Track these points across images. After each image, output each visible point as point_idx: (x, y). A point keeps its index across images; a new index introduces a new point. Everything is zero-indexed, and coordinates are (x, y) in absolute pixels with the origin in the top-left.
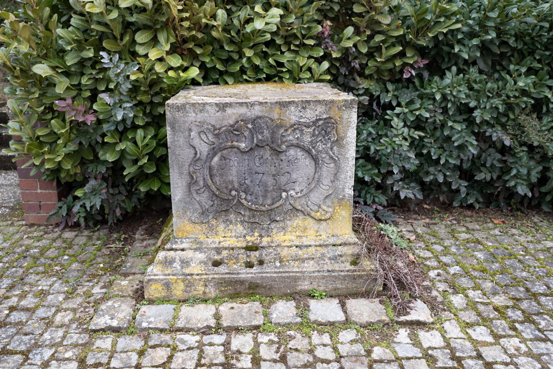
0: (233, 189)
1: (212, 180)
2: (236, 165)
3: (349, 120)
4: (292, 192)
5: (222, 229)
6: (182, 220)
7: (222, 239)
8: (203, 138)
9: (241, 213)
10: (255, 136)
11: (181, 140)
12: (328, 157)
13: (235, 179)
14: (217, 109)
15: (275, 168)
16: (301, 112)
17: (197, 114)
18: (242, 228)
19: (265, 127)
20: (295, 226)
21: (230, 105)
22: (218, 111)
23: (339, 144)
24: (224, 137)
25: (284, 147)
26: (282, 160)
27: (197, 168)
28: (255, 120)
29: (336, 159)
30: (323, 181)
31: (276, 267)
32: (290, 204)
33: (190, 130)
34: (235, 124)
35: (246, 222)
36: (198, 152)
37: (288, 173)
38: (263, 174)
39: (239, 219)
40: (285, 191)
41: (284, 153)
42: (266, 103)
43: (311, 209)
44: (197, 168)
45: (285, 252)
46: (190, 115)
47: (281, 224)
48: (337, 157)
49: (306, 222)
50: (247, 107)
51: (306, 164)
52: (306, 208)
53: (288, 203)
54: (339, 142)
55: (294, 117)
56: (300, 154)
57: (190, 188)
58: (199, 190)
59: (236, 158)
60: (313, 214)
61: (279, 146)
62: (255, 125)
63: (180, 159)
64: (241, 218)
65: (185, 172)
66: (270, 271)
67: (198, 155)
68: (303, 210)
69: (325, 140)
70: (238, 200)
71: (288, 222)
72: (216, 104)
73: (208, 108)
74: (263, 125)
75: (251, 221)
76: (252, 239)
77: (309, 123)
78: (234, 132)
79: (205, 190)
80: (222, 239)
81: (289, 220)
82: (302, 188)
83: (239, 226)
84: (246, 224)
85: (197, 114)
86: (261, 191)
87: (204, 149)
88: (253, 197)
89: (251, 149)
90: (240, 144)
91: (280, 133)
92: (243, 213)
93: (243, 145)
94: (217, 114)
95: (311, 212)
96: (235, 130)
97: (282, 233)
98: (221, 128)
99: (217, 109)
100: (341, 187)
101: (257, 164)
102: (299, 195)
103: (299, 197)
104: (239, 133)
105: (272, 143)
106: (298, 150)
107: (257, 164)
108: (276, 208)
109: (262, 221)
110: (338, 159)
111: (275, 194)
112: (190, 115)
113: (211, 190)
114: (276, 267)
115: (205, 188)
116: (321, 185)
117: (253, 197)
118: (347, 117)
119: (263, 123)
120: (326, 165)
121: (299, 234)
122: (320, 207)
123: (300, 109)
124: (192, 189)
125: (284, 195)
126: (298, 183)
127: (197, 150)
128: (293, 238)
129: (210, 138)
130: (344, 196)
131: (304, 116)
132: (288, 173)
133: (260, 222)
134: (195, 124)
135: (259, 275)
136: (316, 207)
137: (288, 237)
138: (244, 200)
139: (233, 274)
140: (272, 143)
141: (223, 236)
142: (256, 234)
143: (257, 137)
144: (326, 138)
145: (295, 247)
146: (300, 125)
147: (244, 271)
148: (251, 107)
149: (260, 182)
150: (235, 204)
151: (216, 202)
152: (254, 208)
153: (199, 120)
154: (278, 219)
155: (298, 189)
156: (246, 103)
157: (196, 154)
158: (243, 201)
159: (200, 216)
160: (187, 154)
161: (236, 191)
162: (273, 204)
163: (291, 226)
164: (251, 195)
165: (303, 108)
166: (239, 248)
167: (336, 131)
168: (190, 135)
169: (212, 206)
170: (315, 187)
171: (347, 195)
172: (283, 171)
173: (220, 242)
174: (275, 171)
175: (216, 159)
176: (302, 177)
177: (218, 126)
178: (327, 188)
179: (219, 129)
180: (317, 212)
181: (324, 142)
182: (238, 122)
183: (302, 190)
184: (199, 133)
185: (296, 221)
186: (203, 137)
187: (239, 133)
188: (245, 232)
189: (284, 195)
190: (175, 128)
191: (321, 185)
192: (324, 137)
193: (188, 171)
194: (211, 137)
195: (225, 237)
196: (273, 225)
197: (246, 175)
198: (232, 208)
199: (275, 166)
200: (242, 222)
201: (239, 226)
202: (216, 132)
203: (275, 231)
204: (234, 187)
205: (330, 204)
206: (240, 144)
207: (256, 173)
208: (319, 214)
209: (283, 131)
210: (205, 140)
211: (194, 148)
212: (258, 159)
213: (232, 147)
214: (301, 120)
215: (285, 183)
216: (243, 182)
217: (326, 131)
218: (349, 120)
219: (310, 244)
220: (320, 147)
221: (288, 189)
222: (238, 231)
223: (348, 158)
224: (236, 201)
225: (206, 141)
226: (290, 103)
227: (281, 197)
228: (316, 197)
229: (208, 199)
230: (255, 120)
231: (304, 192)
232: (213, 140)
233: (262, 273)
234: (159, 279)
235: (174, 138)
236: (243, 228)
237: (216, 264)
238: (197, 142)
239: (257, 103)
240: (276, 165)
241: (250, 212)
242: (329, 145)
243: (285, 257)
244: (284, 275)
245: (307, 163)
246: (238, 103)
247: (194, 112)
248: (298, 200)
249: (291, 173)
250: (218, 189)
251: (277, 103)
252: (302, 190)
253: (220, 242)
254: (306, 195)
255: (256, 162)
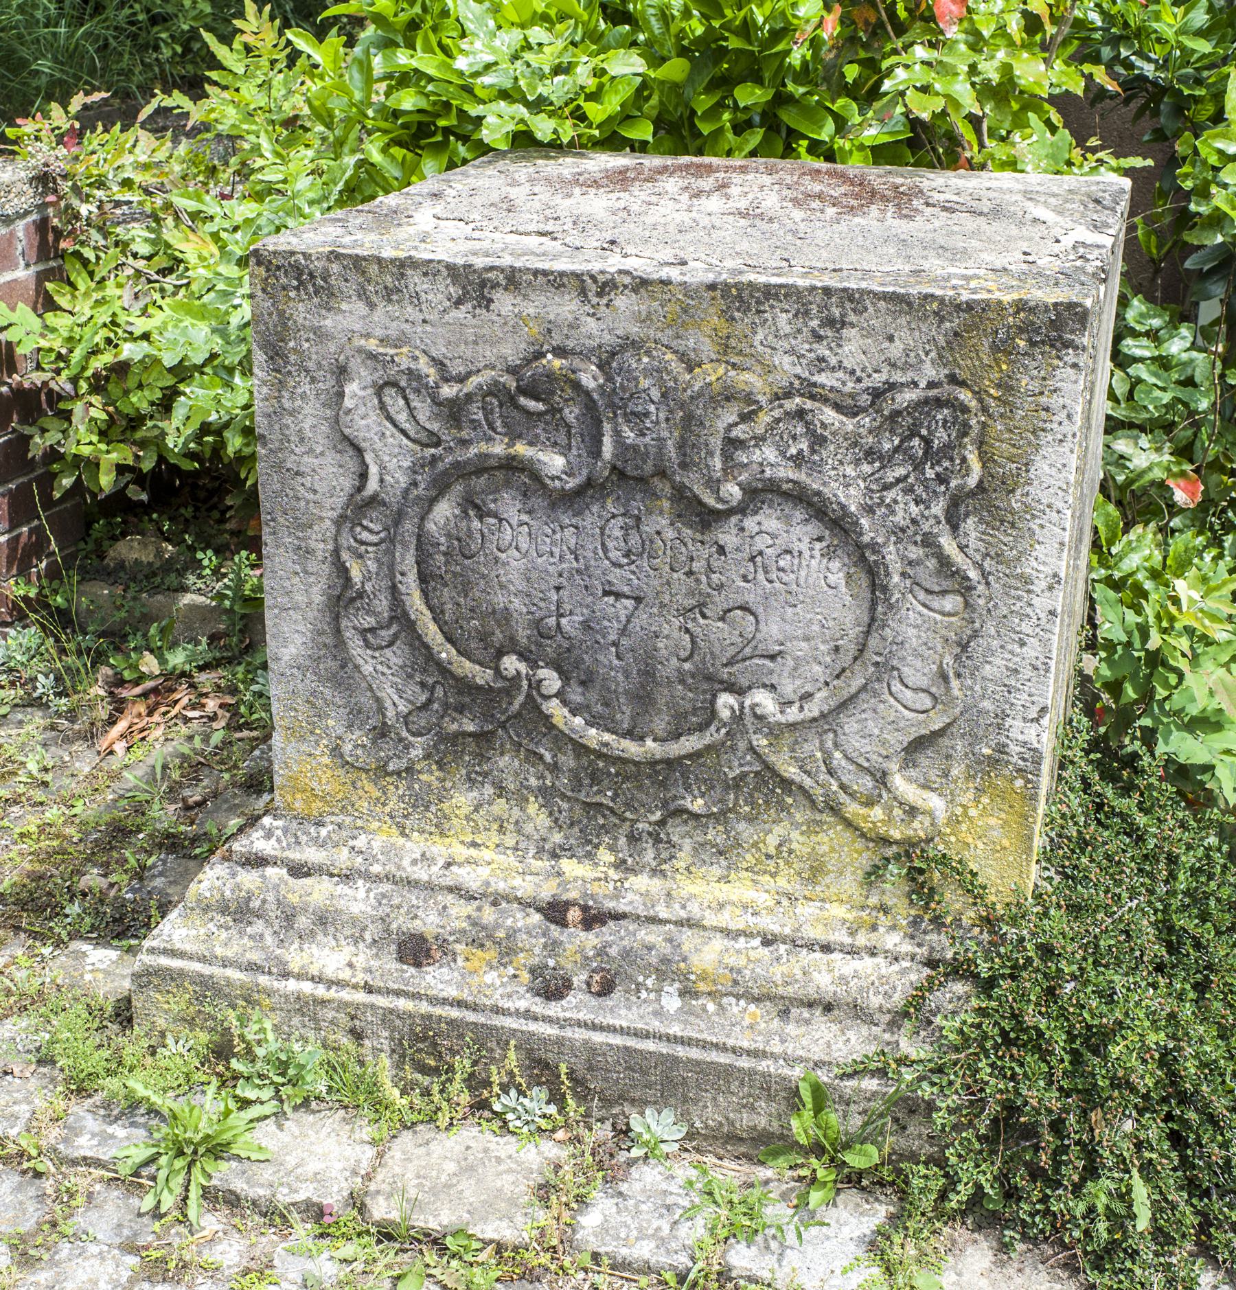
0: (511, 646)
1: (425, 594)
2: (524, 546)
3: (1043, 400)
4: (764, 700)
5: (465, 810)
6: (304, 748)
7: (461, 852)
8: (392, 411)
9: (541, 757)
10: (607, 427)
11: (307, 410)
12: (932, 563)
13: (517, 604)
14: (455, 291)
15: (691, 581)
16: (819, 338)
17: (372, 306)
18: (543, 820)
19: (655, 394)
20: (772, 851)
21: (513, 280)
22: (459, 302)
23: (991, 508)
24: (480, 416)
25: (732, 491)
26: (722, 550)
27: (365, 536)
28: (613, 354)
29: (973, 574)
30: (906, 670)
31: (658, 1013)
32: (752, 749)
33: (342, 372)
34: (528, 361)
35: (563, 796)
36: (373, 470)
37: (745, 608)
38: (638, 600)
39: (533, 782)
40: (731, 688)
41: (734, 520)
42: (666, 283)
43: (843, 787)
44: (365, 536)
45: (707, 955)
46: (344, 306)
47: (715, 834)
48: (979, 566)
49: (822, 837)
50: (583, 292)
51: (832, 579)
52: (823, 777)
53: (742, 745)
54: (989, 500)
55: (787, 359)
56: (801, 533)
57: (337, 618)
58: (372, 630)
59: (525, 518)
60: (852, 809)
61: (714, 485)
62: (609, 379)
63: (302, 492)
64: (541, 777)
65: (322, 549)
66: (644, 1018)
67: (372, 485)
68: (808, 782)
69: (925, 483)
70: (529, 696)
71: (742, 826)
72: (451, 267)
73: (416, 280)
74: (645, 383)
75: (582, 796)
76: (580, 875)
77: (852, 396)
78: (523, 400)
79: (395, 637)
80: (461, 852)
81: (750, 819)
82: (809, 688)
83: (532, 808)
84: (565, 805)
85: (372, 306)
86: (627, 676)
87: (392, 462)
88: (593, 696)
89: (589, 483)
90: (542, 456)
91: (721, 425)
92: (548, 757)
93: (553, 462)
94: (454, 314)
95: (843, 797)
96: (530, 394)
97: (716, 871)
98: (469, 374)
99: (455, 291)
100: (986, 704)
101: (614, 555)
102: (793, 714)
103: (792, 726)
104: (541, 407)
105: (684, 466)
106: (799, 515)
107: (614, 555)
108: (689, 756)
109: (628, 805)
110: (985, 575)
111: (685, 697)
112: (344, 306)
113: (419, 637)
114: (658, 1013)
115: (395, 628)
116: (897, 687)
117: (593, 696)
118: (1035, 386)
119: (647, 372)
120: (922, 595)
121: (789, 888)
122: (882, 779)
123: (815, 323)
124: (344, 623)
125: (726, 701)
126: (790, 663)
127: (369, 458)
128: (764, 899)
129: (422, 418)
130: (1001, 749)
131: (833, 361)
132: (745, 608)
133: (618, 807)
134: (360, 350)
135: (579, 1034)
136: (868, 782)
137: (741, 890)
138: (555, 702)
139: (475, 1008)
140: (684, 466)
141: (469, 839)
142: (605, 856)
143: (617, 433)
144: (930, 473)
145: (757, 942)
146: (812, 397)
147: (522, 1004)
148: (600, 295)
149: (623, 631)
150: (518, 715)
151: (439, 692)
152: (594, 745)
153: (379, 332)
154: (698, 805)
155: (789, 688)
156: (577, 276)
157: (364, 476)
158: (555, 709)
159: (374, 742)
160: (327, 479)
161: (522, 656)
162: (677, 736)
163: (755, 845)
164: (583, 683)
165: (830, 322)
166: (525, 904)
167: (360, 489)
168: (341, 395)
169: (425, 706)
170: (864, 688)
171: (1014, 749)
172: (720, 601)
173: (448, 865)
174: (691, 593)
175: (444, 510)
176: (807, 639)
177: (456, 368)
178: (925, 701)
179: (462, 379)
180: (869, 803)
181: (919, 490)
182: (540, 355)
183: (807, 696)
184: (379, 390)
185: (778, 830)
186: (396, 404)
187: (541, 407)
188: (557, 838)
189: (726, 701)
190: (285, 357)
191: (897, 687)
192: (918, 467)
193: (330, 547)
194: (424, 410)
195: (474, 845)
196: (675, 831)
197: (564, 593)
198: (503, 725)
199: (690, 573)
200: (547, 794)
201: (532, 808)
202: (447, 391)
203: (683, 858)
204: (512, 639)
205: (933, 775)
206: (542, 456)
207: (606, 593)
208: (877, 813)
209: (733, 418)
210: (402, 418)
211: (359, 451)
212: (618, 533)
213: (511, 465)
214: (821, 379)
215: (731, 651)
216: (552, 621)
217: (927, 442)
218: (1043, 400)
219: (832, 938)
220: (899, 508)
221: (744, 682)
222: (528, 828)
223: (1027, 580)
224: (520, 699)
225: (406, 426)
226: (769, 292)
227: (714, 713)
228: (869, 734)
229: (410, 676)
230: (613, 354)
231: (813, 709)
232: (435, 426)
233: (595, 1027)
234: (181, 973)
235: (278, 398)
236: (548, 822)
237: (416, 951)
238: (366, 424)
239: (627, 280)
240: (697, 566)
241: (578, 757)
242: (938, 508)
243: (703, 977)
244: (681, 1051)
245: (837, 578)
246: (545, 273)
247: (362, 294)
248: (788, 738)
249: (760, 611)
250: (450, 640)
251: (712, 287)
252: (807, 696)
253: (448, 865)
254: (826, 721)
255: (610, 544)
